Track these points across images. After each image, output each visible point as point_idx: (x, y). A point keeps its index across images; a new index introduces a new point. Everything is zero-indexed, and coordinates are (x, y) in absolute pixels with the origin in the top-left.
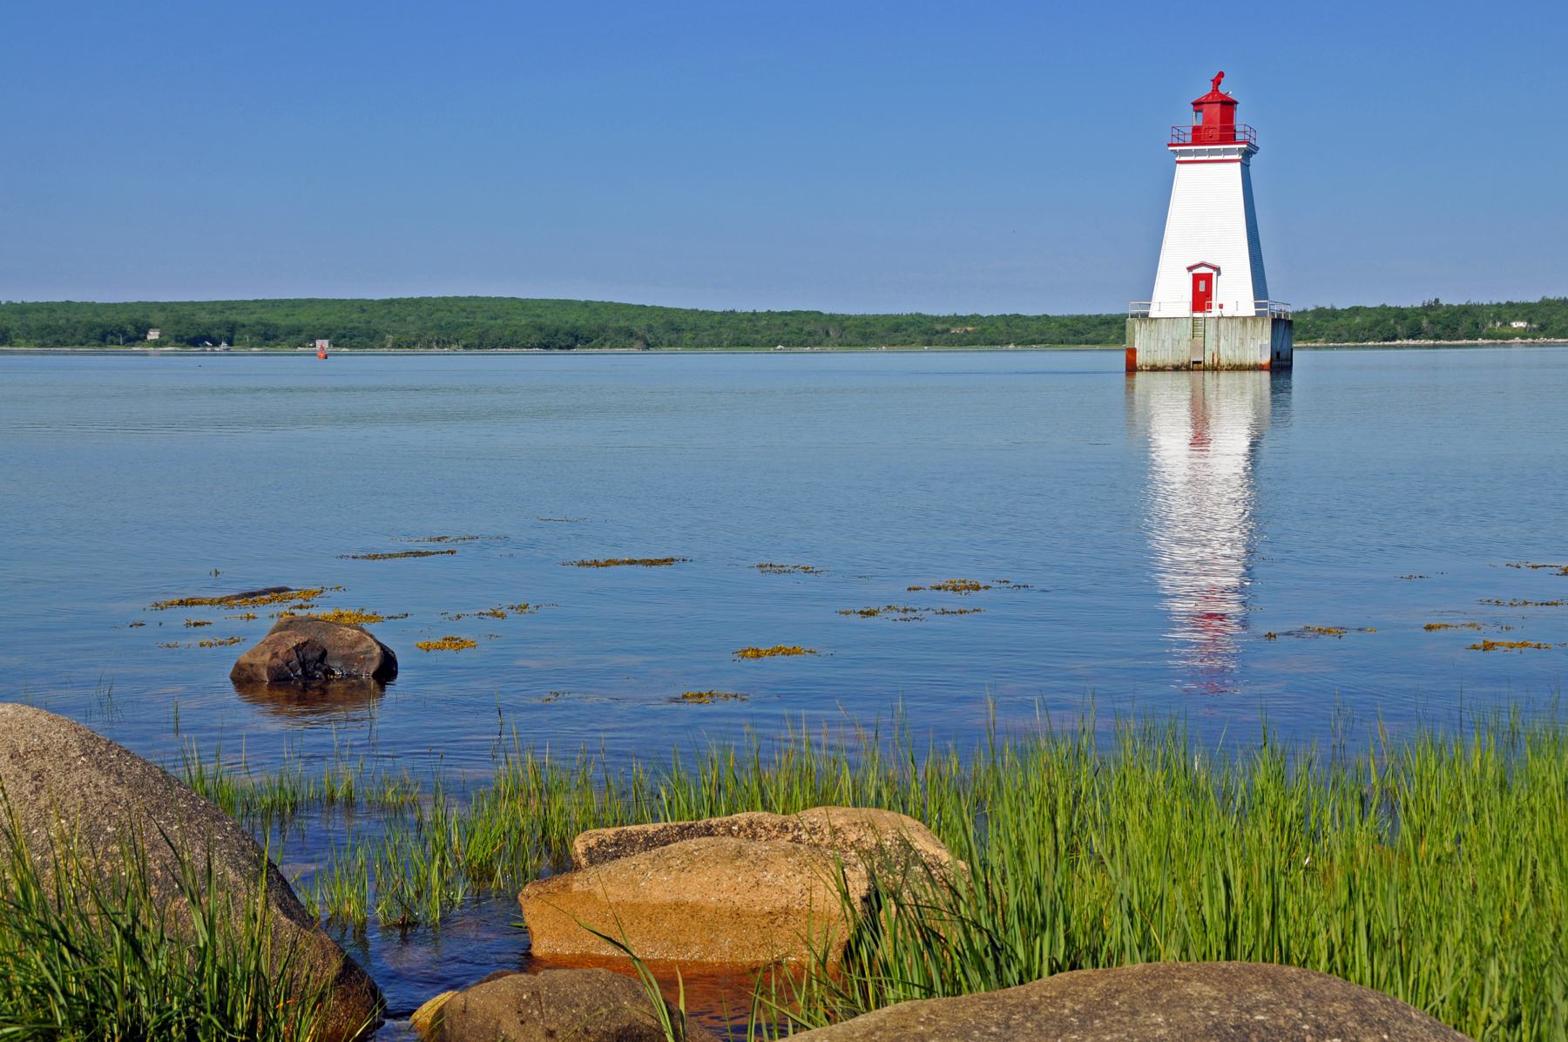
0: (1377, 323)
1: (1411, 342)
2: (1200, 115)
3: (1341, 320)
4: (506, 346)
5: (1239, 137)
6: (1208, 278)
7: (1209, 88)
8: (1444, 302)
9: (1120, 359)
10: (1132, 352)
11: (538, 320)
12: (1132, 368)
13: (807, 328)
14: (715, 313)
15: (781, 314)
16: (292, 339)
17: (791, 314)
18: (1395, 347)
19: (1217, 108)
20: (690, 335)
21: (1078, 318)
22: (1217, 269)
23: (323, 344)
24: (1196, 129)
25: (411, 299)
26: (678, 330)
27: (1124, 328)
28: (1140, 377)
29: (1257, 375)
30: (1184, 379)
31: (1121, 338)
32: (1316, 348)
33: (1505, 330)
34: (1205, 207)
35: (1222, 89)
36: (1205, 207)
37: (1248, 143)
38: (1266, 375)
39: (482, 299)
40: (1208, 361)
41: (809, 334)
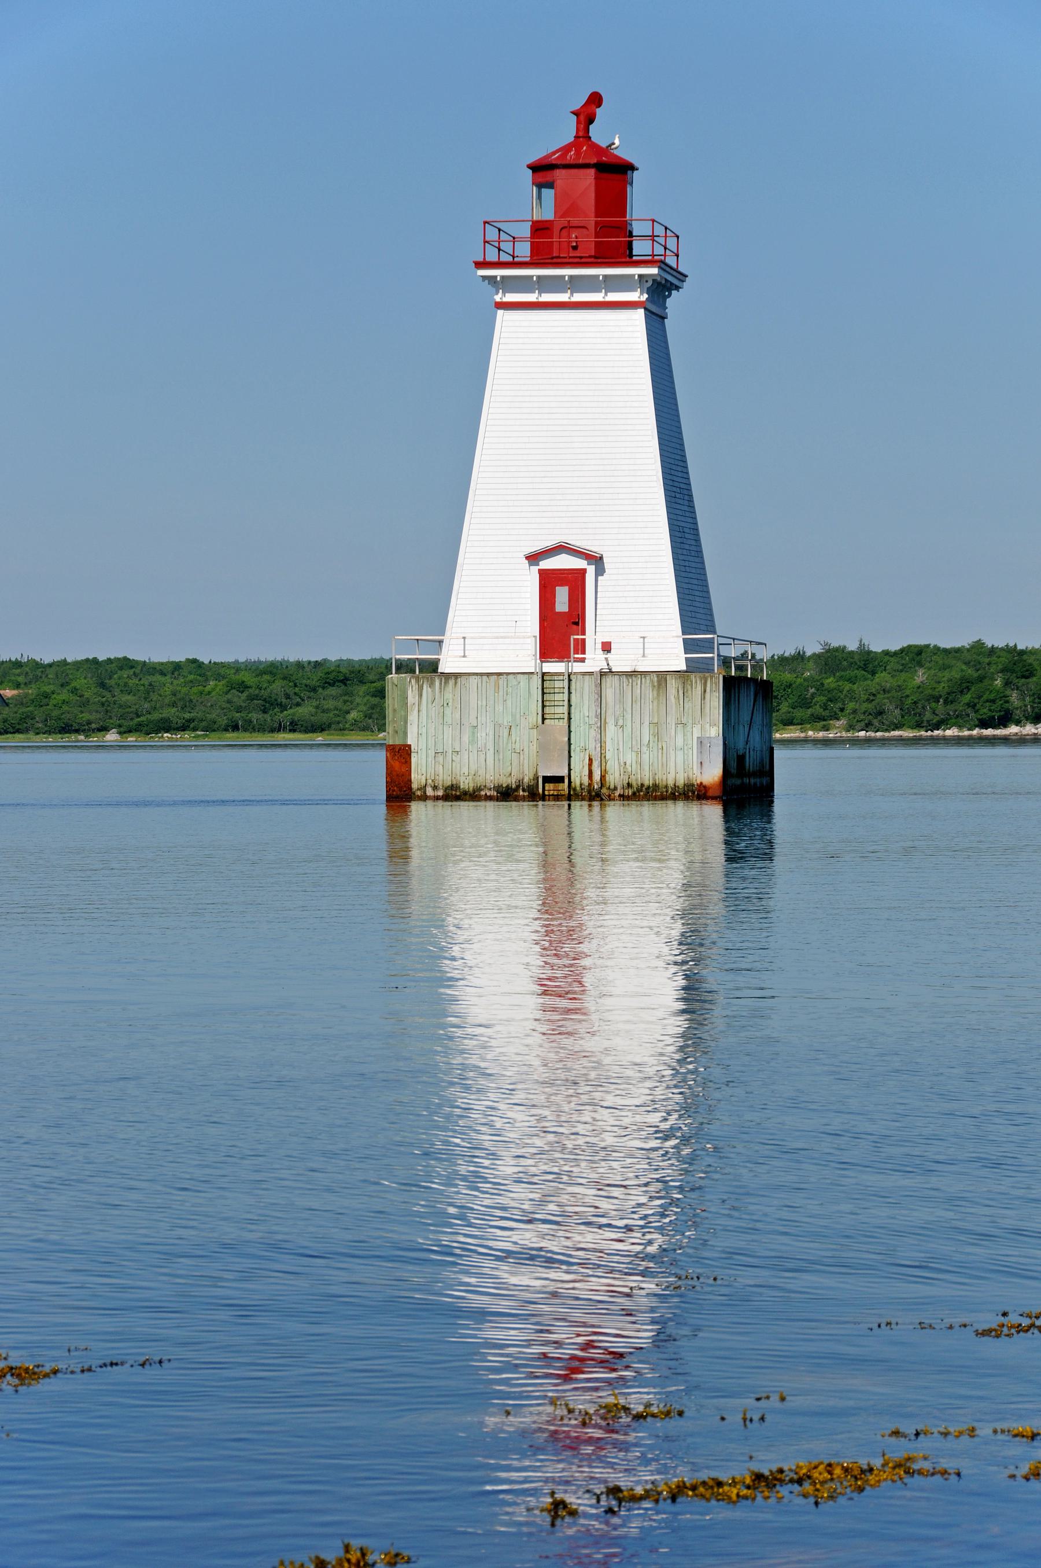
0: (964, 685)
2: (548, 194)
3: (883, 678)
5: (640, 248)
6: (575, 580)
7: (567, 132)
9: (370, 769)
10: (401, 754)
12: (400, 794)
18: (1006, 740)
19: (588, 179)
21: (273, 670)
22: (597, 560)
24: (540, 229)
27: (381, 693)
28: (420, 814)
30: (522, 817)
31: (375, 717)
32: (826, 743)
35: (598, 134)
36: (565, 406)
37: (662, 264)
38: (714, 812)
40: (580, 776)
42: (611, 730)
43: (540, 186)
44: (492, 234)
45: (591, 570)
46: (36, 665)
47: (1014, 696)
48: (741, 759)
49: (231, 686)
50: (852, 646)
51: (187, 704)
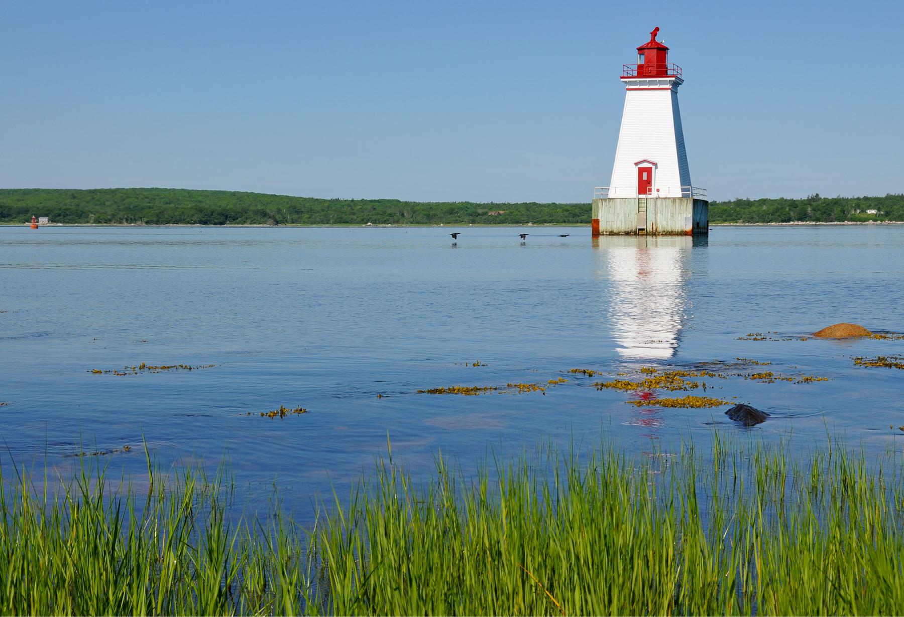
0: (778, 210)
1: (800, 223)
2: (643, 57)
3: (754, 208)
4: (177, 222)
5: (670, 72)
6: (649, 171)
7: (648, 39)
8: (822, 196)
11: (200, 205)
12: (596, 233)
13: (388, 211)
14: (325, 201)
15: (371, 201)
16: (22, 217)
17: (378, 201)
19: (654, 52)
20: (307, 216)
22: (655, 164)
23: (43, 220)
25: (110, 190)
26: (298, 212)
29: (684, 238)
30: (633, 239)
33: (863, 215)
34: (646, 119)
35: (657, 39)
38: (689, 239)
39: (160, 190)
40: (649, 229)
41: (390, 215)
42: (659, 215)
43: (640, 54)
44: (626, 69)
45: (654, 167)
46: (509, 204)
47: (792, 213)
48: (698, 224)
49: (564, 210)
50: (745, 199)
51: (551, 215)
